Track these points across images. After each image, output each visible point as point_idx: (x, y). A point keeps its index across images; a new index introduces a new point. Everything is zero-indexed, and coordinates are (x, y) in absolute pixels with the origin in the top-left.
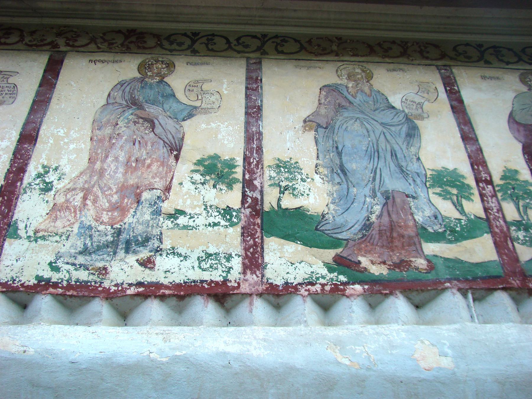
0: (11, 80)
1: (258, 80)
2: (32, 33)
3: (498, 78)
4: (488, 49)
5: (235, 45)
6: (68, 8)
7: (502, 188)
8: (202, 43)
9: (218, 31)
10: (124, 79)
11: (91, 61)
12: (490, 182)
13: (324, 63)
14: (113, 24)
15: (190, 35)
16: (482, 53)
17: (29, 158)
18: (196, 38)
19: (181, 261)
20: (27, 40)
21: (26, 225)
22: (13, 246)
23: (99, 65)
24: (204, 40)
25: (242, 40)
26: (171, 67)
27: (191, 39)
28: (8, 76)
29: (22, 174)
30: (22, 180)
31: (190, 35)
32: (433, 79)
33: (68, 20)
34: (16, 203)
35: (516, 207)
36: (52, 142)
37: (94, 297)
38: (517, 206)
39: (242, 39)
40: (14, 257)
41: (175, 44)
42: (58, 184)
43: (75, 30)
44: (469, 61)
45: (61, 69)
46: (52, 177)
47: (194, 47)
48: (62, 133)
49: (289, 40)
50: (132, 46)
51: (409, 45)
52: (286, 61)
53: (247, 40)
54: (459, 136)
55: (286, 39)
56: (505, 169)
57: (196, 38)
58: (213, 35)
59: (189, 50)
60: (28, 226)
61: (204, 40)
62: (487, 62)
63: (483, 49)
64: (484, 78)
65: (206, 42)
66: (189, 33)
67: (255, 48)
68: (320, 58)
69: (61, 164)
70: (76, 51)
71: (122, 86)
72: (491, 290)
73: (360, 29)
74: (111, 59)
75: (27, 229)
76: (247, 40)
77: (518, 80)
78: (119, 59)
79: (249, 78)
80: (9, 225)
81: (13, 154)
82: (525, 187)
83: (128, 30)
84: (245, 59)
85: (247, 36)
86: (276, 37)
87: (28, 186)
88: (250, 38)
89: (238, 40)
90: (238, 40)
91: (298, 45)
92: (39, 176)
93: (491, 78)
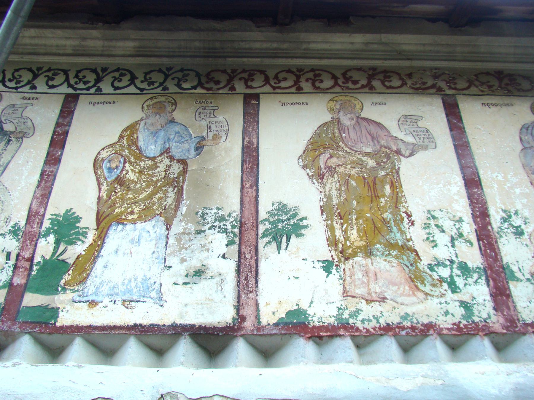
0: (420, 124)
1: (71, 113)
2: (410, 76)
6: (431, 50)
10: (526, 122)
11: (90, 103)
14: (479, 66)
17: (486, 203)
19: (125, 279)
20: (409, 82)
21: (519, 268)
22: (518, 288)
23: (493, 109)
25: (349, 74)
27: (296, 75)
28: (416, 121)
29: (487, 219)
30: (490, 224)
33: (436, 62)
34: (498, 246)
36: (496, 186)
37: (474, 334)
39: (348, 73)
40: (525, 299)
41: (350, 82)
42: (527, 228)
43: (447, 72)
45: (460, 112)
46: (517, 221)
48: (500, 177)
49: (391, 74)
52: (415, 95)
53: (356, 75)
60: (521, 268)
63: (501, 76)
65: (383, 79)
66: (294, 70)
69: (517, 208)
70: (463, 94)
71: (527, 130)
74: (501, 102)
75: (522, 271)
76: (356, 75)
77: (529, 111)
78: (508, 102)
80: (503, 267)
81: (469, 199)
83: (495, 72)
87: (500, 230)
88: (285, 72)
89: (208, 75)
90: (344, 75)
92: (504, 220)
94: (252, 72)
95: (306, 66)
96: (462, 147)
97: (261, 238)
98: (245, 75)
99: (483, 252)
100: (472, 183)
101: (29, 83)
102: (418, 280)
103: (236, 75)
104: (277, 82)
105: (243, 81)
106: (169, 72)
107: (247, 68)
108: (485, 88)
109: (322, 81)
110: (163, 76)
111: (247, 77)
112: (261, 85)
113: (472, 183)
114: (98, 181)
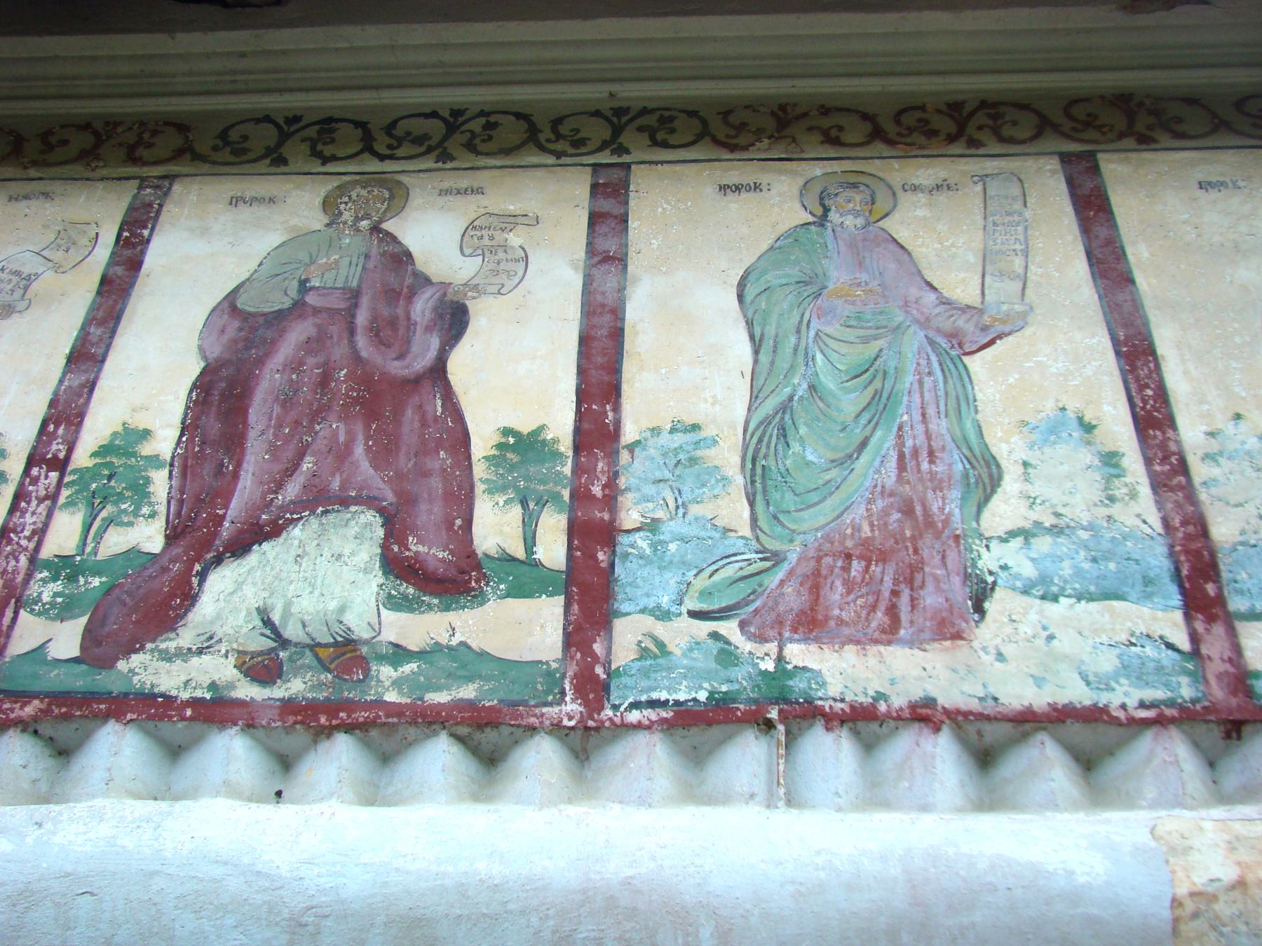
3: (757, 187)
4: (972, 114)
5: (548, 141)
7: (80, 478)
8: (303, 140)
9: (341, 108)
11: (724, 188)
12: (61, 465)
13: (496, 173)
15: (609, 114)
16: (1131, 118)
18: (293, 129)
24: (981, 118)
26: (397, 197)
31: (609, 114)
32: (1045, 187)
35: (84, 523)
38: (89, 520)
44: (237, 160)
47: (281, 150)
50: (982, 136)
51: (119, 130)
54: (67, 351)
55: (492, 119)
56: (120, 429)
57: (293, 129)
58: (330, 120)
59: (268, 161)
61: (312, 132)
62: (973, 143)
64: (235, 201)
67: (598, 144)
68: (925, 152)
72: (327, 732)
73: (31, 98)
79: (595, 219)
82: (141, 471)
84: (589, 170)
85: (582, 113)
86: (645, 111)
91: (868, 127)
93: (254, 200)
94: (667, 114)
95: (473, 103)
96: (1109, 267)
97: (60, 509)
98: (651, 120)
99: (295, 516)
100: (1136, 354)
101: (268, 152)
102: (913, 634)
103: (297, 131)
104: (395, 143)
105: (308, 143)
106: (619, 119)
107: (650, 105)
108: (918, 138)
109: (672, 131)
110: (274, 132)
111: (315, 135)
112: (354, 150)
113: (1136, 354)
114: (869, 404)
